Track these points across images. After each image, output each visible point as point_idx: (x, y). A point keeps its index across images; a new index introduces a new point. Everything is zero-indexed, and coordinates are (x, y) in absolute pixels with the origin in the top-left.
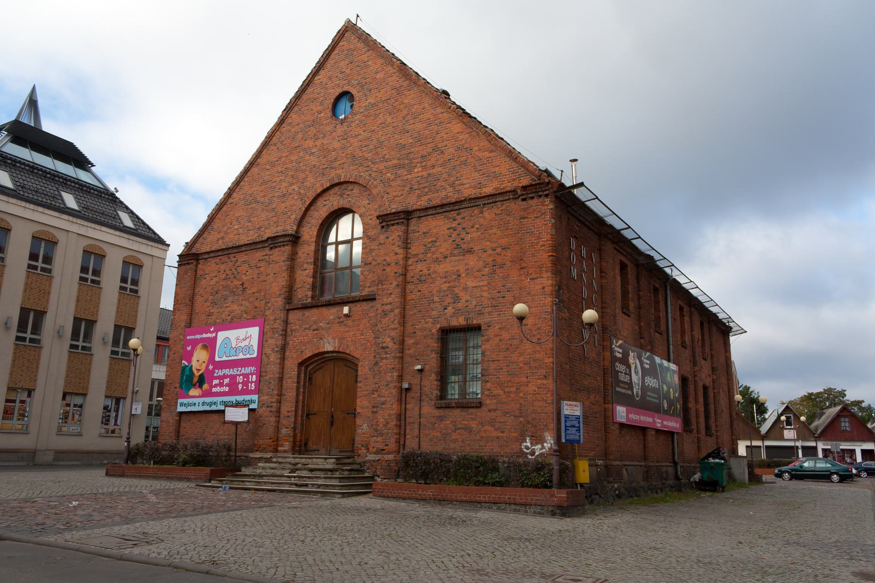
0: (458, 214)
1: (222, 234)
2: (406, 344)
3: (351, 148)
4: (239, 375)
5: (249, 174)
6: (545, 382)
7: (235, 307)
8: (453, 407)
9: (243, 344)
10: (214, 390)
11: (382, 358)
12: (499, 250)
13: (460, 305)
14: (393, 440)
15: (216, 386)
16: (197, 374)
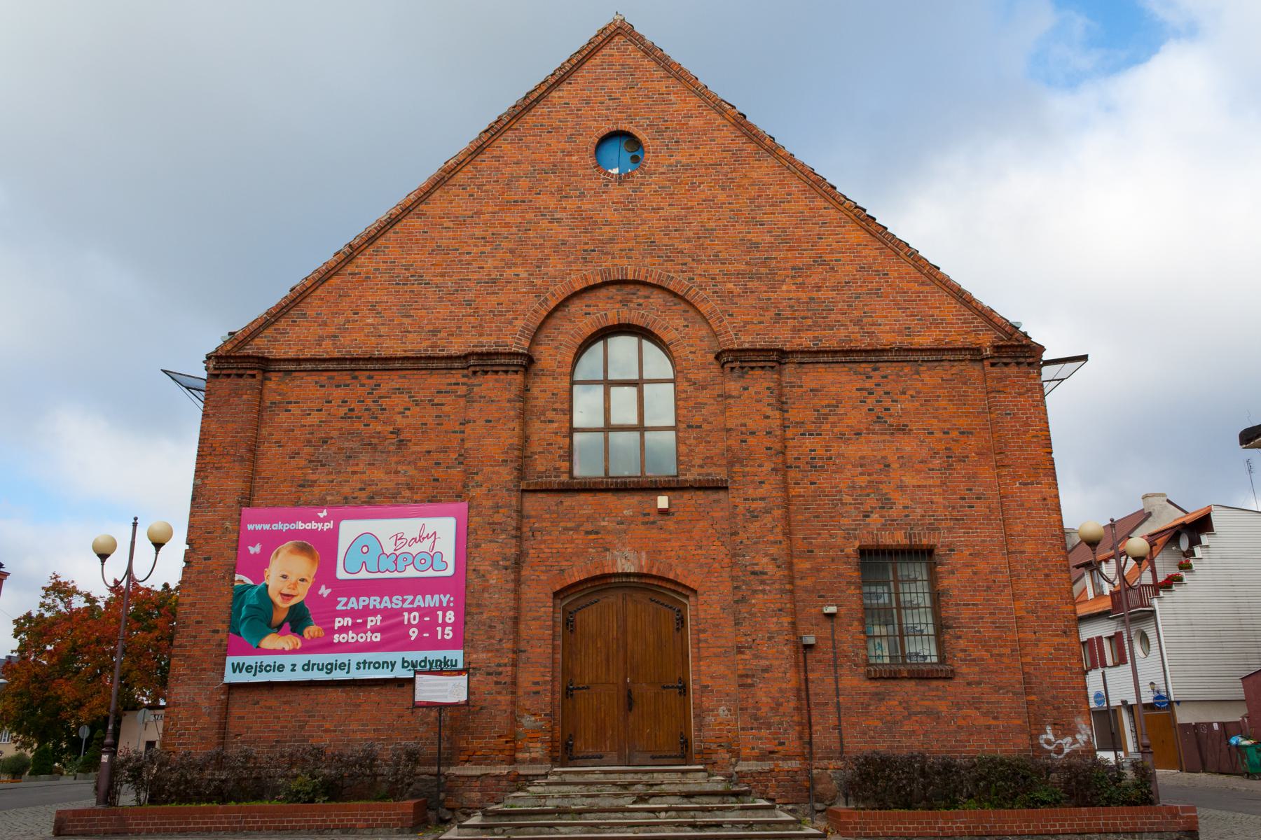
0: (875, 369)
1: (331, 330)
2: (796, 568)
3: (646, 227)
4: (410, 611)
5: (397, 227)
6: (1065, 641)
7: (378, 474)
8: (903, 678)
9: (415, 549)
10: (336, 638)
11: (755, 591)
12: (955, 434)
13: (893, 513)
14: (793, 735)
15: (343, 630)
16: (284, 605)
